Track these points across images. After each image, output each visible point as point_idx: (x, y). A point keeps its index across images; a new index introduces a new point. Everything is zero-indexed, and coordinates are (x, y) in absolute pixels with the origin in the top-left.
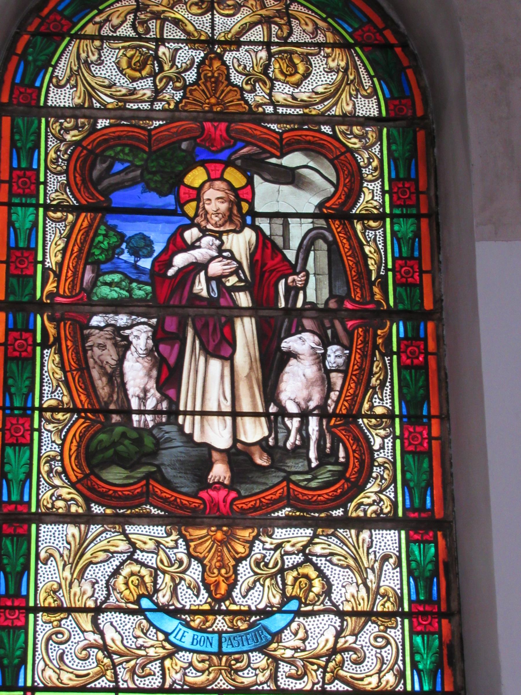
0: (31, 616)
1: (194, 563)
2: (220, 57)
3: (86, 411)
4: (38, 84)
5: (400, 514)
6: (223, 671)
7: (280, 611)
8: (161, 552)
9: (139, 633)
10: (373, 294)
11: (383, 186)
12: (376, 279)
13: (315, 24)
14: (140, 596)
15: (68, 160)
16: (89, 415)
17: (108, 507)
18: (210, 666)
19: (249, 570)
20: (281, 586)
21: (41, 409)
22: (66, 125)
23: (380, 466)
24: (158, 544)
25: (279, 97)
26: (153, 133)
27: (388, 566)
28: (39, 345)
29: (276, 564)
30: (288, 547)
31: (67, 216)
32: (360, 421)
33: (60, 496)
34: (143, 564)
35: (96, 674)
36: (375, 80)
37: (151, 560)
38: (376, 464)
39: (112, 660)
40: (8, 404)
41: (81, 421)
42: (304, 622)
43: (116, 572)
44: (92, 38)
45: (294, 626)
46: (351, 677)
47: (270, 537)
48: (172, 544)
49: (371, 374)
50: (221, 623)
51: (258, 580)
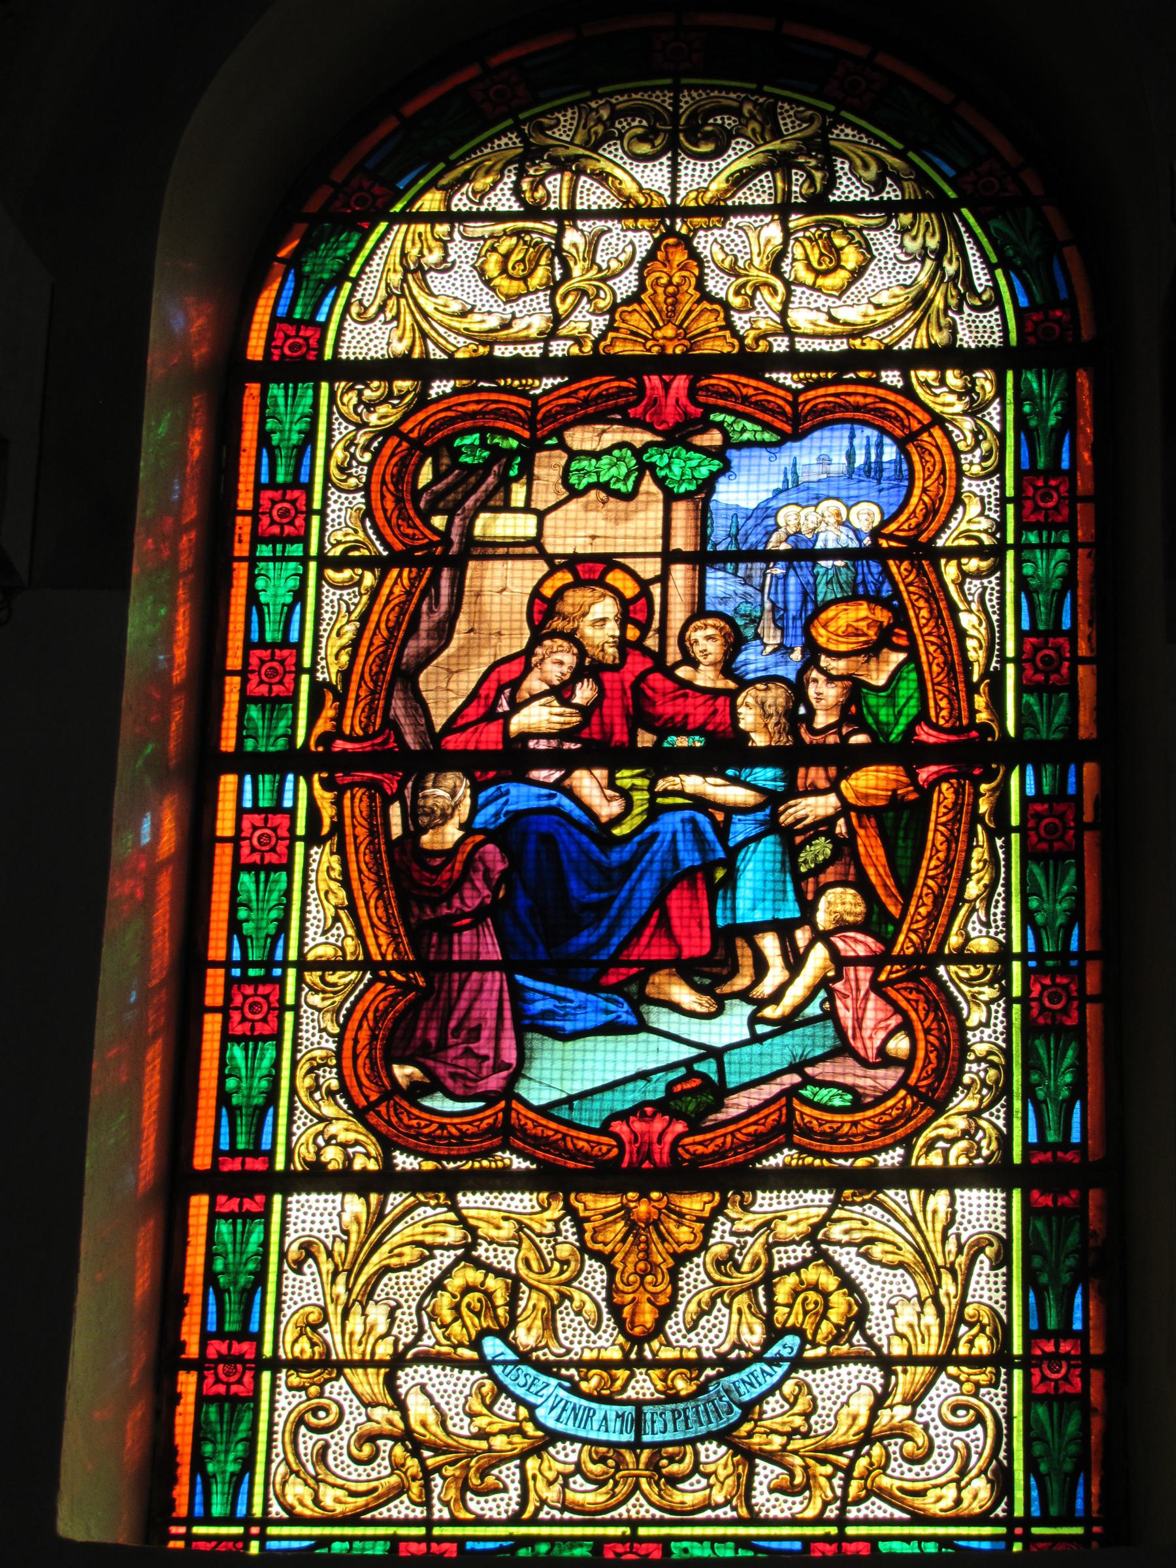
0: (266, 1376)
1: (591, 1264)
2: (686, 242)
3: (385, 964)
4: (321, 318)
5: (1017, 1158)
6: (643, 1481)
7: (758, 1358)
8: (526, 1244)
9: (477, 1407)
10: (973, 712)
11: (1002, 487)
12: (982, 678)
13: (881, 163)
14: (484, 1333)
15: (371, 465)
16: (394, 974)
17: (428, 1157)
18: (618, 1470)
19: (703, 1276)
20: (764, 1309)
21: (303, 965)
22: (368, 393)
23: (978, 1060)
24: (521, 1226)
25: (799, 318)
26: (541, 401)
27: (984, 1262)
28: (300, 838)
29: (756, 1264)
30: (783, 1229)
31: (362, 576)
32: (941, 970)
33: (334, 1137)
34: (489, 1269)
35: (391, 1488)
36: (999, 273)
37: (508, 1260)
38: (971, 1057)
39: (422, 1461)
40: (236, 955)
41: (380, 986)
42: (809, 1380)
43: (437, 1285)
44: (432, 218)
45: (789, 1387)
46: (901, 1489)
47: (746, 1209)
48: (550, 1228)
49: (966, 874)
50: (644, 1385)
51: (721, 1295)
